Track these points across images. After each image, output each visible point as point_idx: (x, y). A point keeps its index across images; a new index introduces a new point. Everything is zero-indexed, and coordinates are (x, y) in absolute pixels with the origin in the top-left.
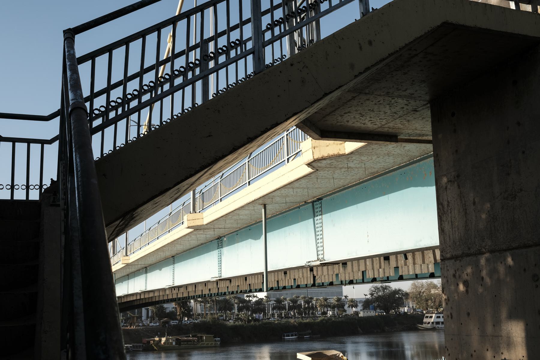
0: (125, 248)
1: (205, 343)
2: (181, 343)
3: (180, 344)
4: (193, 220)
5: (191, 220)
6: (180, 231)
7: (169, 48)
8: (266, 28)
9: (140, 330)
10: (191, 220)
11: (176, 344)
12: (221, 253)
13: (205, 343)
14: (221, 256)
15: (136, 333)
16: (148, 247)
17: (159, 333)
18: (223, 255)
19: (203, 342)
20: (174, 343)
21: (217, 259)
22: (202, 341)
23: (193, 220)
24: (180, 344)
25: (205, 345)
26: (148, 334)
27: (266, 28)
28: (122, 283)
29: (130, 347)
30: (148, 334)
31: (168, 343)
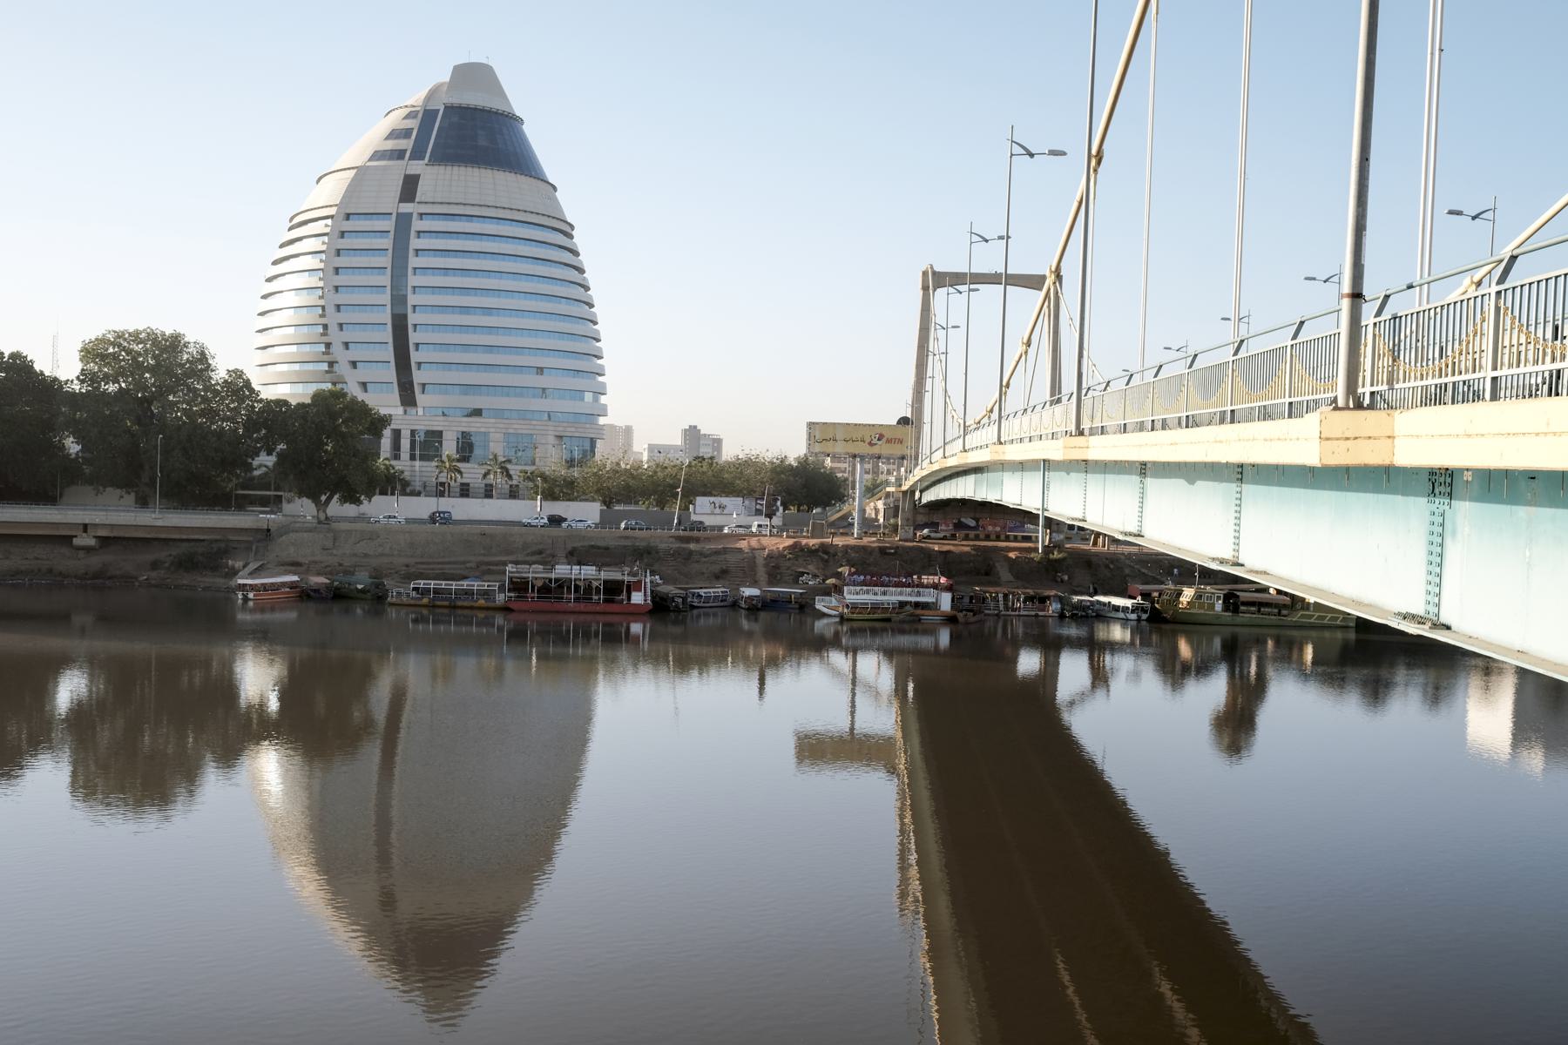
0: (1075, 396)
1: (1313, 616)
2: (1239, 608)
3: (1236, 610)
4: (1347, 439)
5: (1337, 439)
6: (1279, 439)
7: (1049, 289)
8: (310, 401)
9: (1123, 557)
10: (1337, 439)
11: (1226, 608)
12: (1442, 525)
13: (1313, 616)
14: (1442, 535)
15: (1112, 566)
16: (1146, 436)
17: (1176, 570)
18: (1454, 533)
19: (1308, 609)
20: (1219, 606)
21: (1425, 562)
22: (1302, 609)
23: (1347, 439)
24: (1236, 610)
25: (1312, 620)
26: (1143, 570)
27: (310, 401)
28: (1068, 474)
29: (1088, 604)
30: (1146, 571)
31: (1201, 606)
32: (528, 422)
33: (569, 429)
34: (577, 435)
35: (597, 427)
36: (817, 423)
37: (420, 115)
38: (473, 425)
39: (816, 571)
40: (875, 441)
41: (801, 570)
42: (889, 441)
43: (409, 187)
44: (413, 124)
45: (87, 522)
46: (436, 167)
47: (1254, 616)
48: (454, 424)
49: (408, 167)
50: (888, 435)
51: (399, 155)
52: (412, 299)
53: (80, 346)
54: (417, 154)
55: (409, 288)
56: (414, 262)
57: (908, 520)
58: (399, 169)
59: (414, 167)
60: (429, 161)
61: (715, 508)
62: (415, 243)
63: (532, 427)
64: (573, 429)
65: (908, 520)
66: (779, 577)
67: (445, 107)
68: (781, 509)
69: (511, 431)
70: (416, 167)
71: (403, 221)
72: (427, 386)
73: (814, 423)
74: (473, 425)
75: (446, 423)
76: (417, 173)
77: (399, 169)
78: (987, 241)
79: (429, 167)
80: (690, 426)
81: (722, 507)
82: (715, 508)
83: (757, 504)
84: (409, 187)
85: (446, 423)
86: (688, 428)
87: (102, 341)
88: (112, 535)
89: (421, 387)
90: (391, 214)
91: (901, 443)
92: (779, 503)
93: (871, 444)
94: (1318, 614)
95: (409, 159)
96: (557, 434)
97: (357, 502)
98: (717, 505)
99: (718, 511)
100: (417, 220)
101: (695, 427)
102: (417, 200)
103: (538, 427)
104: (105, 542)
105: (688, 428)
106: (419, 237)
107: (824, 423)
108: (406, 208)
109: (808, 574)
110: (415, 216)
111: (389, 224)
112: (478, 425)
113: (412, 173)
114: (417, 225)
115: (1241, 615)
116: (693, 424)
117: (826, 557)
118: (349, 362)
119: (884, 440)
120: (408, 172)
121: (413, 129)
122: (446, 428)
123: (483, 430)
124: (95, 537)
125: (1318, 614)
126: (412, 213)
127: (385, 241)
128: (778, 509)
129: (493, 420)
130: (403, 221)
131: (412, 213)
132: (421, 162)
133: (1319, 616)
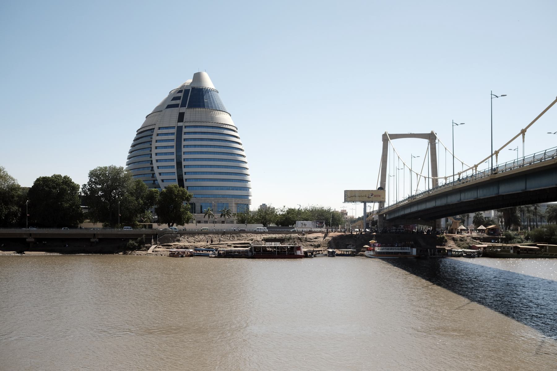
1: (549, 254)
32: (225, 199)
33: (239, 201)
34: (242, 203)
35: (248, 200)
36: (349, 191)
37: (183, 92)
38: (206, 200)
39: (353, 244)
40: (370, 196)
41: (347, 243)
42: (375, 196)
43: (181, 117)
44: (181, 95)
45: (95, 233)
46: (190, 109)
47: (526, 254)
48: (200, 200)
49: (180, 110)
50: (374, 194)
51: (176, 106)
52: (184, 157)
53: (89, 172)
54: (183, 105)
55: (182, 153)
56: (184, 143)
57: (381, 225)
58: (175, 112)
59: (182, 110)
60: (188, 107)
61: (303, 225)
62: (184, 136)
63: (227, 200)
64: (241, 201)
65: (381, 225)
66: (339, 246)
67: (192, 88)
68: (325, 225)
69: (219, 202)
70: (183, 110)
71: (180, 129)
72: (189, 187)
73: (347, 191)
74: (206, 200)
75: (196, 200)
76: (184, 112)
77: (175, 112)
78: (498, 97)
79: (187, 109)
80: (263, 204)
81: (305, 225)
82: (303, 225)
83: (317, 224)
84: (181, 117)
85: (196, 200)
86: (262, 205)
87: (95, 170)
88: (103, 237)
89: (187, 188)
90: (175, 127)
91: (380, 196)
92: (324, 223)
93: (368, 197)
94: (550, 253)
95: (181, 107)
96: (236, 203)
97: (183, 225)
98: (303, 224)
99: (304, 226)
100: (184, 128)
101: (265, 204)
102: (184, 121)
103: (229, 201)
104: (100, 240)
105: (262, 205)
106: (185, 134)
107: (351, 190)
108: (180, 124)
109: (350, 245)
110: (183, 127)
111: (174, 131)
112: (208, 200)
113: (182, 112)
114: (185, 130)
115: (521, 254)
116: (264, 203)
117: (356, 239)
118: (161, 180)
119: (374, 195)
120: (180, 112)
121: (181, 96)
122: (197, 202)
123: (210, 202)
124: (97, 238)
125: (550, 253)
126: (182, 126)
127: (173, 136)
128: (324, 226)
129: (213, 199)
130: (180, 129)
131: (182, 126)
132: (185, 108)
133: (551, 254)
